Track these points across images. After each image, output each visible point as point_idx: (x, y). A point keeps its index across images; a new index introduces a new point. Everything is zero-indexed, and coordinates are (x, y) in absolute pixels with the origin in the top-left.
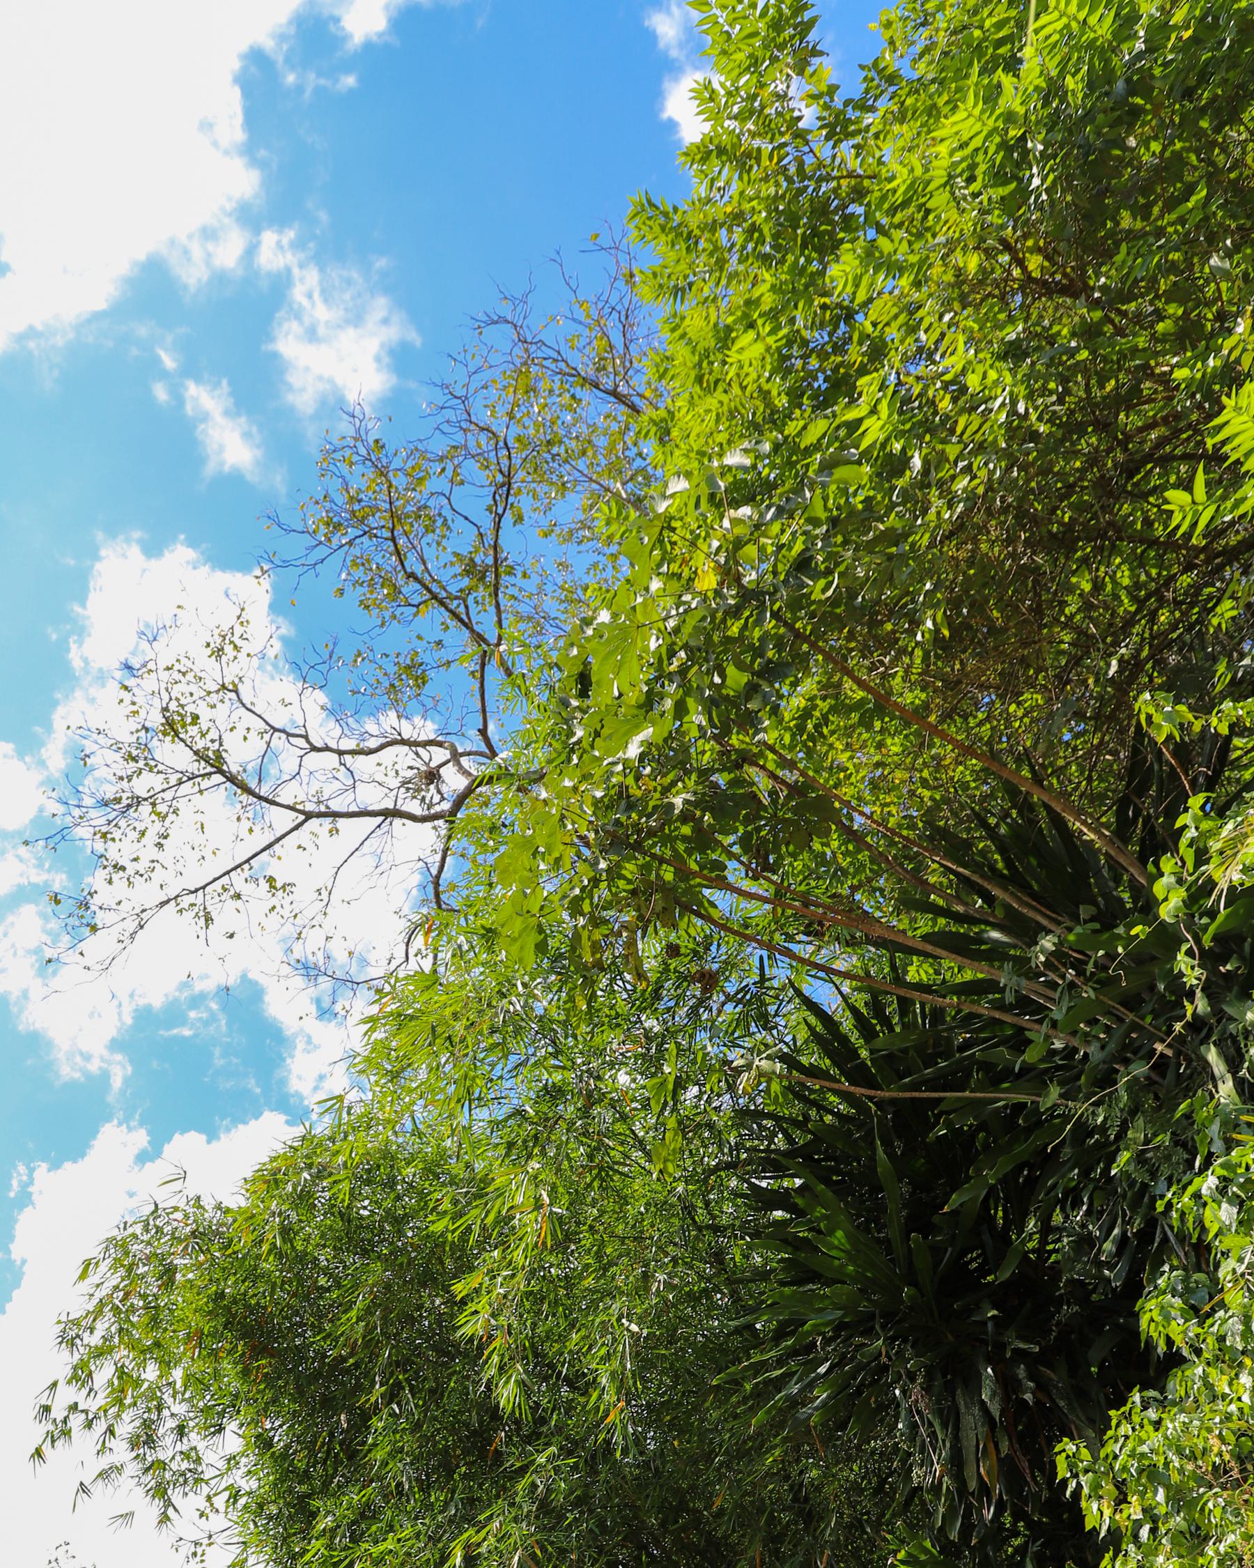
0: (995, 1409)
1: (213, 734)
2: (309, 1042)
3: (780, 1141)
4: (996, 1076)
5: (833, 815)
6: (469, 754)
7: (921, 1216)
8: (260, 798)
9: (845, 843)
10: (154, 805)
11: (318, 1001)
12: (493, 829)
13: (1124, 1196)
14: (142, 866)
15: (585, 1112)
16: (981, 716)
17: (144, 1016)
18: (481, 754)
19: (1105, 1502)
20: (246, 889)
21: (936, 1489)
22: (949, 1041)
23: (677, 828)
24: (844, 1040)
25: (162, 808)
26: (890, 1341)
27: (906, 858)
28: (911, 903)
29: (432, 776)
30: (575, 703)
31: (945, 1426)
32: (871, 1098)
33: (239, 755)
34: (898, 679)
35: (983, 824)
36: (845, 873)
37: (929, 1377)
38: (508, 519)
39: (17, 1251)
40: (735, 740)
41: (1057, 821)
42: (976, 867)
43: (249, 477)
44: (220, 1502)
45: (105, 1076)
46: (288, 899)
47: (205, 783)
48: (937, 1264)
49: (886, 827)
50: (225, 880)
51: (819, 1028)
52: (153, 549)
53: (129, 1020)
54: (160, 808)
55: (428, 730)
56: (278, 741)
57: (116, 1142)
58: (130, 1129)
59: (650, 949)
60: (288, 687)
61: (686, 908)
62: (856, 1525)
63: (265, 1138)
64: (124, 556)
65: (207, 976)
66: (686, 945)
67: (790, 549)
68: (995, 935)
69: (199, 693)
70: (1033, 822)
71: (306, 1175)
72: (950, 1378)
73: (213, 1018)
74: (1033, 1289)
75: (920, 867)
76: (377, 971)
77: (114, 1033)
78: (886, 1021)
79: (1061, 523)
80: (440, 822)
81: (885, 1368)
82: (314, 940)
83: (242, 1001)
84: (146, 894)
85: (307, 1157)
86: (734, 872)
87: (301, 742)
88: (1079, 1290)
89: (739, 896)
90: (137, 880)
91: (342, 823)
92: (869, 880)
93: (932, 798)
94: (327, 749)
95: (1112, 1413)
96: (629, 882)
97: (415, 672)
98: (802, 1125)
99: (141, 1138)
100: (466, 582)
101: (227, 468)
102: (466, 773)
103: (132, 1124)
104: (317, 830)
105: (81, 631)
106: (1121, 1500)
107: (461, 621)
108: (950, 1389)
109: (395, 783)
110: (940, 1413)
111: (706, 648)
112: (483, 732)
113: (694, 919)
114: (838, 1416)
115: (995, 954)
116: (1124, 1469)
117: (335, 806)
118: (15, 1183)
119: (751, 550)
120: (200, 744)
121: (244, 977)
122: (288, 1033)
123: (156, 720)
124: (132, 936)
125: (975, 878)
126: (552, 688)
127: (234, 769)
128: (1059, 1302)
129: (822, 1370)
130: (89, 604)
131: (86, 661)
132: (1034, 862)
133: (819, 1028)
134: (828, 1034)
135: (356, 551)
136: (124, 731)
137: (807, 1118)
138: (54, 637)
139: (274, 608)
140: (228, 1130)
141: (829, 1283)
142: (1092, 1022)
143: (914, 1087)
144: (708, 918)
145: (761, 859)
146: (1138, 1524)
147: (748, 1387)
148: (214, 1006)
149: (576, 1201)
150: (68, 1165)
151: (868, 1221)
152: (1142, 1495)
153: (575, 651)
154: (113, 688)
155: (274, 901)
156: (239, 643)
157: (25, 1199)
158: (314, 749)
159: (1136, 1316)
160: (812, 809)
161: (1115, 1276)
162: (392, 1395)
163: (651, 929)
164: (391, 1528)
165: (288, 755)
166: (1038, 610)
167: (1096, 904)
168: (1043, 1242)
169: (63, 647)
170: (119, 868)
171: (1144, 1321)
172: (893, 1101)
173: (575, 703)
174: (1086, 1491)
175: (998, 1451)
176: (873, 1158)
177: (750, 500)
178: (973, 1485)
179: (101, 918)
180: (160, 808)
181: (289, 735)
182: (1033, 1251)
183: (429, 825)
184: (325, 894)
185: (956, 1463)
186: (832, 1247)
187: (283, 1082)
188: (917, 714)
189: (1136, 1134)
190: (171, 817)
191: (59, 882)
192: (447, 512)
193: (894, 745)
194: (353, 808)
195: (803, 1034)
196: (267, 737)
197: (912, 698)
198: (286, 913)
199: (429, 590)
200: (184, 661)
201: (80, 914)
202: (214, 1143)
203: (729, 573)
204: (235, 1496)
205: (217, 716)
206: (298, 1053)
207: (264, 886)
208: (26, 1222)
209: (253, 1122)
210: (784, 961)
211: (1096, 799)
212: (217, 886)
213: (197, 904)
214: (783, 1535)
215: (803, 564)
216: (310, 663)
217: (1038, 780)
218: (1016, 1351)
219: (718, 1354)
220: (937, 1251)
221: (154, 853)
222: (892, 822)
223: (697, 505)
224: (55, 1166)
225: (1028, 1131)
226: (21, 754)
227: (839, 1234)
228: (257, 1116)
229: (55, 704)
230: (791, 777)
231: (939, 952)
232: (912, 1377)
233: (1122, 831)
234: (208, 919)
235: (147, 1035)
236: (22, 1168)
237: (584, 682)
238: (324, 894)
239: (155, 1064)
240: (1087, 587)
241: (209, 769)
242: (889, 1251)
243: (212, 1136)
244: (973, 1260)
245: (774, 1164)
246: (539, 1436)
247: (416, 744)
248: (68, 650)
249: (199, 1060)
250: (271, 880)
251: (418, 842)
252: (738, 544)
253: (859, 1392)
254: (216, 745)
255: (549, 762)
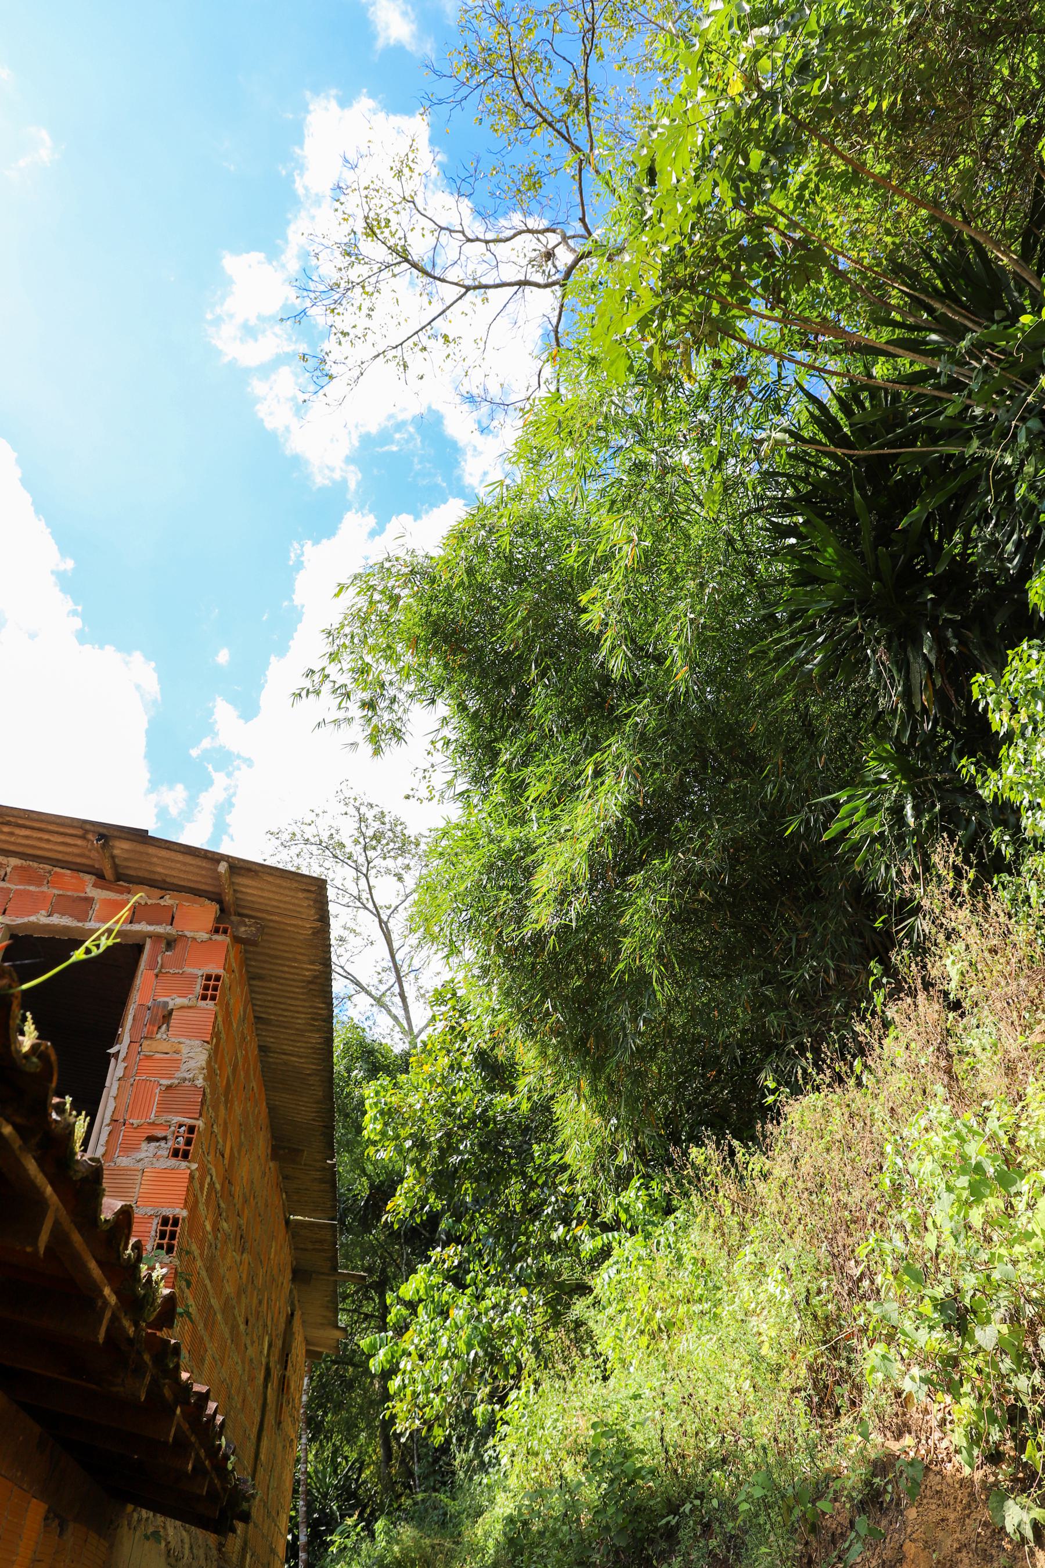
0: (932, 658)
1: (400, 234)
2: (475, 449)
3: (790, 492)
4: (934, 437)
5: (825, 260)
6: (573, 237)
7: (884, 534)
8: (435, 278)
9: (833, 279)
10: (363, 287)
11: (479, 422)
12: (593, 287)
13: (1020, 512)
14: (359, 332)
15: (660, 479)
16: (928, 178)
17: (367, 440)
18: (582, 236)
19: (1004, 713)
20: (430, 344)
21: (894, 712)
22: (904, 413)
23: (719, 277)
24: (833, 420)
25: (369, 289)
26: (864, 618)
27: (875, 287)
28: (880, 320)
29: (549, 255)
30: (646, 190)
31: (899, 671)
32: (850, 457)
33: (419, 250)
34: (870, 155)
35: (928, 257)
36: (833, 301)
37: (889, 640)
38: (593, 57)
39: (298, 599)
40: (756, 210)
41: (981, 252)
42: (924, 290)
43: (408, 48)
44: (439, 745)
45: (345, 481)
46: (458, 348)
47: (397, 270)
48: (894, 566)
49: (862, 265)
50: (415, 338)
51: (817, 412)
52: (345, 102)
53: (357, 444)
54: (367, 289)
55: (544, 224)
56: (445, 236)
57: (355, 525)
58: (363, 515)
59: (700, 365)
60: (450, 200)
61: (726, 334)
62: (842, 738)
63: (453, 512)
64: (326, 109)
65: (405, 409)
66: (725, 358)
67: (794, 58)
68: (934, 337)
69: (387, 204)
70: (963, 254)
71: (483, 532)
72: (904, 640)
73: (411, 438)
74: (959, 578)
75: (886, 294)
76: (517, 395)
77: (347, 452)
78: (861, 404)
79: (989, 22)
80: (557, 287)
81: (861, 636)
82: (477, 377)
83: (430, 425)
84: (364, 351)
85: (482, 520)
86: (758, 304)
87: (460, 236)
88: (989, 579)
89: (759, 325)
90: (357, 341)
91: (491, 292)
92: (849, 306)
93: (893, 243)
94: (478, 239)
95: (1009, 652)
96: (687, 317)
97: (534, 180)
98: (804, 479)
99: (371, 521)
100: (566, 109)
101: (392, 42)
102: (573, 250)
103: (366, 511)
104: (474, 300)
105: (301, 168)
106: (1014, 711)
107: (564, 137)
108: (903, 647)
109: (525, 262)
110: (896, 663)
111: (735, 140)
112: (582, 220)
113: (733, 342)
114: (827, 674)
115: (936, 352)
116: (1016, 690)
117: (484, 281)
118: (292, 555)
119: (765, 63)
120: (391, 242)
121: (429, 409)
122: (461, 444)
123: (360, 226)
124: (356, 381)
125: (922, 297)
126: (630, 180)
127: (416, 258)
128: (975, 587)
129: (820, 640)
130: (306, 147)
131: (306, 188)
132: (962, 282)
133: (817, 412)
134: (824, 420)
135: (488, 89)
136: (341, 234)
137: (808, 474)
138: (284, 173)
139: (432, 141)
140: (427, 512)
141: (825, 582)
142: (1001, 393)
143: (881, 447)
144: (741, 340)
145: (775, 293)
146: (1024, 727)
147: (772, 655)
148: (412, 429)
149: (658, 538)
150: (324, 541)
151: (849, 542)
152: (1028, 706)
153: (645, 151)
154: (328, 204)
155: (449, 351)
156: (413, 165)
157: (299, 565)
158: (469, 240)
159: (1026, 592)
160: (809, 258)
161: (1012, 567)
162: (543, 674)
163: (702, 350)
164: (547, 757)
165: (451, 245)
166: (970, 95)
167: (1006, 309)
168: (965, 547)
169: (290, 180)
170: (345, 334)
171: (1031, 594)
172: (866, 459)
173: (646, 190)
174: (991, 706)
175: (933, 684)
176: (851, 499)
177: (765, 22)
178: (918, 708)
179: (334, 370)
180: (367, 289)
181: (451, 231)
182: (958, 554)
183: (548, 290)
184: (481, 345)
185: (907, 695)
186: (825, 559)
187: (459, 478)
188: (882, 181)
189: (1028, 469)
190: (376, 295)
191: (303, 348)
192: (551, 55)
193: (867, 204)
194: (498, 281)
195: (804, 417)
196: (436, 234)
197: (881, 169)
198: (457, 358)
199: (541, 116)
200: (376, 181)
201: (320, 371)
202: (419, 522)
203: (751, 81)
204: (448, 743)
205: (402, 220)
206: (468, 457)
207: (441, 340)
208: (302, 580)
209: (442, 506)
210: (791, 366)
211: (1008, 234)
212: (410, 342)
213: (397, 355)
214: (794, 749)
215: (803, 68)
216: (460, 181)
217: (967, 221)
218: (946, 620)
219: (750, 635)
220: (894, 557)
221: (366, 322)
222: (866, 262)
223: (730, 26)
224: (317, 542)
225: (955, 473)
226: (269, 261)
227: (830, 550)
228: (445, 501)
229: (288, 223)
230: (798, 235)
231: (899, 351)
232: (878, 641)
233: (1026, 255)
234: (405, 366)
235: (370, 451)
236: (296, 545)
237: (652, 174)
238: (482, 343)
239: (375, 471)
240: (1006, 72)
241: (399, 259)
242: (863, 560)
243: (417, 517)
244: (918, 564)
245: (786, 507)
246: (637, 693)
247: (538, 232)
248: (294, 182)
249: (405, 465)
250: (445, 337)
251: (543, 303)
252: (757, 56)
253: (843, 654)
254: (402, 242)
255: (631, 234)
